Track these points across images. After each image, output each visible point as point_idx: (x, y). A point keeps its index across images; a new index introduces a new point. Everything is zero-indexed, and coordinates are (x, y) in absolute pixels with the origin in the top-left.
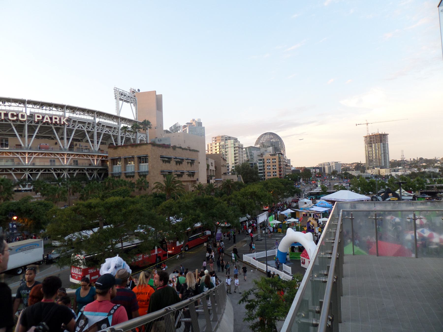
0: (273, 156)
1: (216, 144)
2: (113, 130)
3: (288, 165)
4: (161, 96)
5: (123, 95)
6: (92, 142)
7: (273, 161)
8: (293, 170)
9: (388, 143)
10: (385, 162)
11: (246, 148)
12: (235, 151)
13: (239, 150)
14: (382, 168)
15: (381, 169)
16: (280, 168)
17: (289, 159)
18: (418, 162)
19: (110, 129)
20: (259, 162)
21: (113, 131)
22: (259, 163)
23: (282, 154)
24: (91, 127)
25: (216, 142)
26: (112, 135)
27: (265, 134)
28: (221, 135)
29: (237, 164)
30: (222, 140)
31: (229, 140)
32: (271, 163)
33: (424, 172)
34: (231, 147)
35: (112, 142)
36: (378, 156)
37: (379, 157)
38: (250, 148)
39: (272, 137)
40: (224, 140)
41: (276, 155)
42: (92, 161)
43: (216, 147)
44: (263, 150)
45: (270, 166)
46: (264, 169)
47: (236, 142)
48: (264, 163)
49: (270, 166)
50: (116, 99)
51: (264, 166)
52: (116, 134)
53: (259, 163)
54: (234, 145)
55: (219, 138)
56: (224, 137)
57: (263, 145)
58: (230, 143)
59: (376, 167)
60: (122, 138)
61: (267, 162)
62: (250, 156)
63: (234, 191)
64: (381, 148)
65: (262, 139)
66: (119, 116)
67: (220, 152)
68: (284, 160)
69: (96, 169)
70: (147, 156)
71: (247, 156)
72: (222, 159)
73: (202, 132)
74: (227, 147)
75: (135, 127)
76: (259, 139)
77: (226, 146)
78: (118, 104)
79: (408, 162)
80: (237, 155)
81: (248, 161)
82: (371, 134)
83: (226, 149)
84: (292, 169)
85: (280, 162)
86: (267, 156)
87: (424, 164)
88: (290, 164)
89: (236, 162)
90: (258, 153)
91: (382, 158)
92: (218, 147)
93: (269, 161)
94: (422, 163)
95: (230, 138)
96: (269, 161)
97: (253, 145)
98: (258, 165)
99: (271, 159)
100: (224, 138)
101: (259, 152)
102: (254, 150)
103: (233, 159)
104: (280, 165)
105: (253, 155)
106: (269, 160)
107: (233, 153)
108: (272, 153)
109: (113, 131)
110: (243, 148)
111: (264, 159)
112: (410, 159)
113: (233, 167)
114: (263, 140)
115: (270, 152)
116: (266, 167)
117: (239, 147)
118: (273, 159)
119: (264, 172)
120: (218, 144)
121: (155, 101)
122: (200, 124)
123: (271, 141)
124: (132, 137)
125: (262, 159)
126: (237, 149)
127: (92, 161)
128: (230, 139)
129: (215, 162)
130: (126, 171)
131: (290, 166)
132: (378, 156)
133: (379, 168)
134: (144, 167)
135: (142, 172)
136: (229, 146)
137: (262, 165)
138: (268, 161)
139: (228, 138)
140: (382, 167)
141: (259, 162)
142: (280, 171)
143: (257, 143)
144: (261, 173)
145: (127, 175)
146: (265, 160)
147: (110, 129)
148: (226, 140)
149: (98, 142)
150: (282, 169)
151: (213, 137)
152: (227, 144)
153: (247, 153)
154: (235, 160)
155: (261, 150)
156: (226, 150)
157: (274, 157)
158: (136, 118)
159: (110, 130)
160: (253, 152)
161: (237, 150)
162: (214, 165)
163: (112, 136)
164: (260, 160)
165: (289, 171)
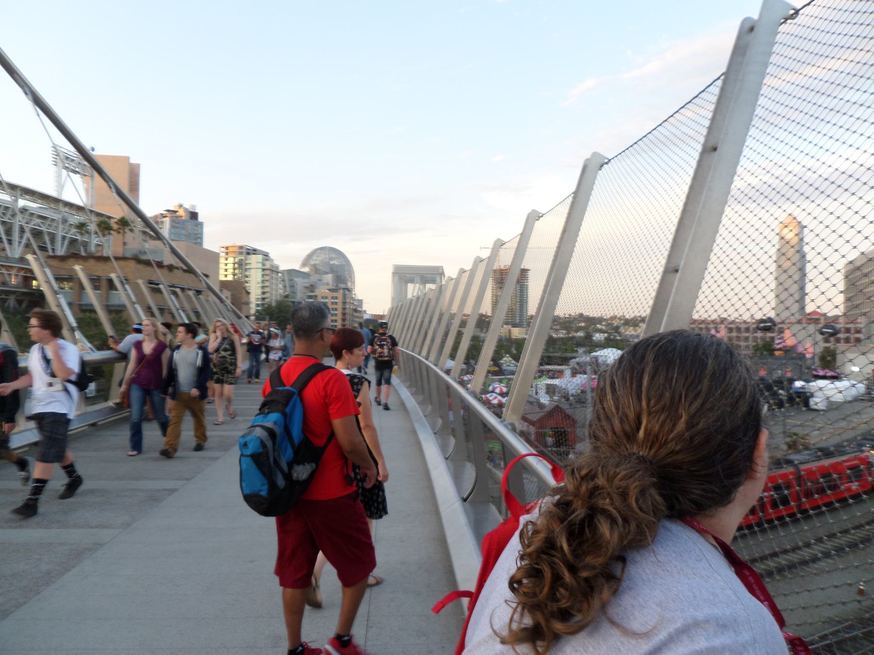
4: (138, 166)
6: (10, 242)
10: (521, 316)
11: (283, 272)
12: (263, 275)
14: (515, 325)
15: (514, 327)
16: (344, 314)
17: (360, 298)
18: (575, 319)
24: (9, 216)
27: (322, 249)
29: (267, 300)
30: (241, 253)
33: (574, 337)
38: (291, 272)
40: (244, 253)
41: (339, 291)
42: (7, 277)
43: (226, 264)
44: (314, 278)
54: (264, 265)
57: (316, 269)
58: (255, 261)
63: (613, 322)
66: (59, 198)
69: (14, 292)
71: (285, 287)
76: (310, 256)
77: (246, 264)
78: (59, 176)
80: (267, 284)
82: (502, 267)
83: (246, 270)
84: (366, 317)
85: (344, 303)
87: (583, 324)
89: (265, 296)
90: (306, 282)
95: (255, 251)
100: (244, 251)
101: (306, 281)
102: (299, 277)
104: (344, 309)
106: (326, 298)
107: (260, 279)
108: (331, 287)
112: (565, 315)
113: (258, 305)
114: (316, 260)
118: (333, 298)
122: (194, 215)
126: (268, 272)
127: (7, 277)
130: (81, 301)
133: (510, 326)
134: (326, 300)
135: (113, 306)
136: (253, 266)
140: (515, 324)
142: (344, 320)
143: (304, 264)
145: (84, 308)
148: (248, 254)
149: (20, 242)
150: (348, 317)
157: (335, 294)
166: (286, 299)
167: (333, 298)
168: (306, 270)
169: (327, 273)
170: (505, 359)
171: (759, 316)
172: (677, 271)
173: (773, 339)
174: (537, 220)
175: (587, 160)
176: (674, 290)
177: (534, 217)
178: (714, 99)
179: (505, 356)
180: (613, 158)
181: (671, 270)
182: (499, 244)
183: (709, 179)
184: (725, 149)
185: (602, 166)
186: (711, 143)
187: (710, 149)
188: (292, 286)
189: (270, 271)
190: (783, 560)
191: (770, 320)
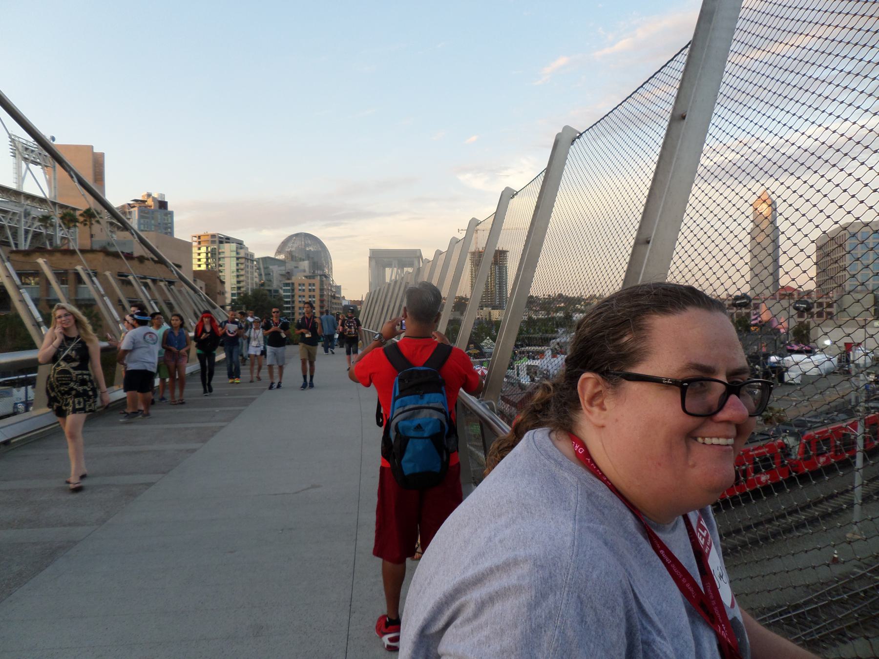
0: (310, 279)
1: (199, 249)
2: (10, 216)
3: (337, 295)
4: (102, 155)
5: (28, 150)
7: (310, 288)
8: (346, 306)
9: (506, 266)
11: (258, 260)
12: (237, 264)
13: (247, 264)
14: (494, 308)
15: (492, 309)
19: (4, 215)
20: (284, 288)
21: (10, 219)
22: (285, 291)
23: (326, 277)
25: (199, 246)
26: (9, 226)
27: (297, 235)
28: (212, 232)
30: (213, 242)
31: (227, 242)
32: (307, 291)
34: (231, 257)
35: (7, 238)
36: (489, 288)
37: (491, 289)
38: (266, 260)
39: (309, 242)
40: (217, 242)
41: (316, 278)
43: (199, 254)
44: (290, 265)
45: (304, 296)
46: (293, 302)
47: (241, 248)
48: (293, 290)
49: (304, 296)
50: (14, 156)
51: (293, 296)
52: (16, 224)
53: (285, 291)
54: (238, 253)
55: (206, 238)
56: (217, 237)
57: (292, 256)
58: (228, 249)
59: (486, 307)
60: (27, 232)
61: (300, 290)
62: (266, 275)
64: (496, 274)
65: (290, 245)
66: (20, 190)
67: (207, 265)
68: (330, 288)
70: (706, 376)
71: (260, 275)
72: (218, 281)
73: (168, 220)
74: (222, 256)
75: (67, 218)
76: (285, 243)
78: (18, 168)
79: (540, 299)
80: (242, 273)
81: (263, 285)
84: (344, 303)
85: (322, 290)
86: (298, 278)
88: (341, 295)
90: (281, 270)
91: (496, 291)
92: (203, 256)
93: (304, 288)
94: (560, 302)
95: (228, 240)
96: (304, 288)
97: (272, 255)
98: (281, 292)
99: (307, 285)
100: (217, 239)
101: (283, 268)
103: (234, 280)
104: (322, 296)
105: (271, 274)
106: (304, 285)
107: (234, 268)
108: (307, 273)
109: (10, 219)
110: (252, 261)
111: (293, 284)
114: (291, 247)
115: (304, 271)
116: (297, 299)
117: (246, 259)
118: (310, 285)
119: (293, 308)
120: (204, 249)
121: (90, 164)
122: (163, 205)
123: (307, 249)
124: (9, 223)
125: (289, 283)
126: (242, 261)
128: (228, 241)
129: (206, 285)
131: (341, 299)
132: (489, 288)
135: (83, 300)
136: (227, 254)
137: (289, 294)
138: (300, 288)
139: (224, 240)
141: (284, 288)
143: (279, 252)
144: (288, 308)
146: (296, 286)
147: (4, 215)
148: (221, 242)
150: (326, 304)
151: (195, 234)
152: (223, 250)
153: (259, 269)
154: (239, 282)
155: (287, 264)
156: (221, 262)
157: (311, 281)
158: (55, 196)
159: (3, 217)
160: (271, 267)
161: (242, 264)
162: (204, 288)
163: (8, 228)
164: (287, 285)
165: (338, 307)
166: (262, 288)
167: (310, 285)
168: (282, 257)
169: (303, 260)
170: (485, 341)
171: (733, 291)
172: (648, 242)
173: (748, 315)
174: (512, 198)
175: (558, 135)
176: (646, 261)
177: (508, 195)
178: (682, 67)
179: (486, 339)
180: (585, 132)
181: (642, 241)
182: (474, 224)
183: (678, 148)
184: (693, 117)
185: (574, 141)
186: (680, 112)
187: (678, 118)
188: (268, 274)
189: (245, 259)
190: (770, 528)
191: (744, 296)
